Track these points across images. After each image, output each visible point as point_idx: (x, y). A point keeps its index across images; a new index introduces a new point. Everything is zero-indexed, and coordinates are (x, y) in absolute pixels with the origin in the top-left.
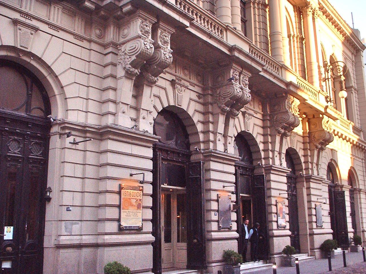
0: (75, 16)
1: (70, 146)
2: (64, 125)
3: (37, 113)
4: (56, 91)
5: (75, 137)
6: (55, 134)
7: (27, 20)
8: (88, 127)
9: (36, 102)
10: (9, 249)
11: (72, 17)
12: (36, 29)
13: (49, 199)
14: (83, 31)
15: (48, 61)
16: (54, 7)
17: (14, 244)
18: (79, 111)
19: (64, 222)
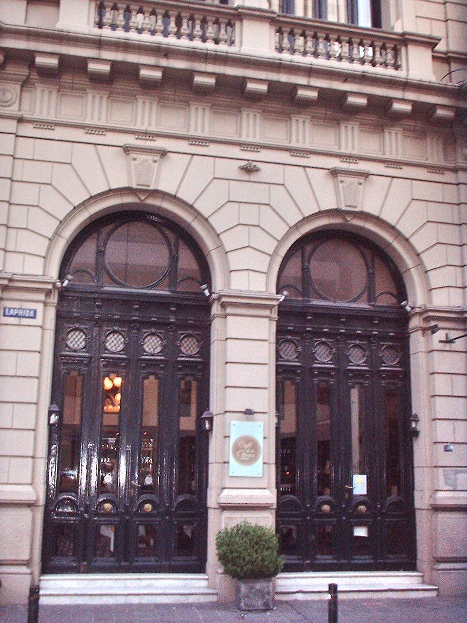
0: (425, 136)
1: (441, 346)
2: (427, 314)
3: (385, 301)
4: (409, 262)
5: (446, 331)
6: (416, 330)
7: (351, 164)
8: (430, 310)
9: (383, 284)
10: (362, 508)
11: (421, 139)
12: (366, 175)
13: (416, 433)
14: (442, 157)
15: (390, 218)
16: (390, 133)
17: (369, 502)
18: (251, 273)
19: (441, 470)
